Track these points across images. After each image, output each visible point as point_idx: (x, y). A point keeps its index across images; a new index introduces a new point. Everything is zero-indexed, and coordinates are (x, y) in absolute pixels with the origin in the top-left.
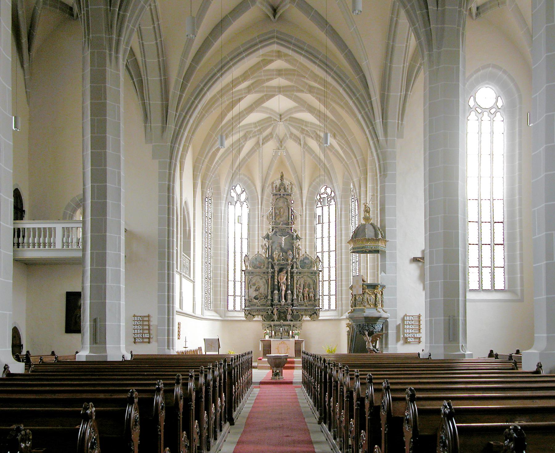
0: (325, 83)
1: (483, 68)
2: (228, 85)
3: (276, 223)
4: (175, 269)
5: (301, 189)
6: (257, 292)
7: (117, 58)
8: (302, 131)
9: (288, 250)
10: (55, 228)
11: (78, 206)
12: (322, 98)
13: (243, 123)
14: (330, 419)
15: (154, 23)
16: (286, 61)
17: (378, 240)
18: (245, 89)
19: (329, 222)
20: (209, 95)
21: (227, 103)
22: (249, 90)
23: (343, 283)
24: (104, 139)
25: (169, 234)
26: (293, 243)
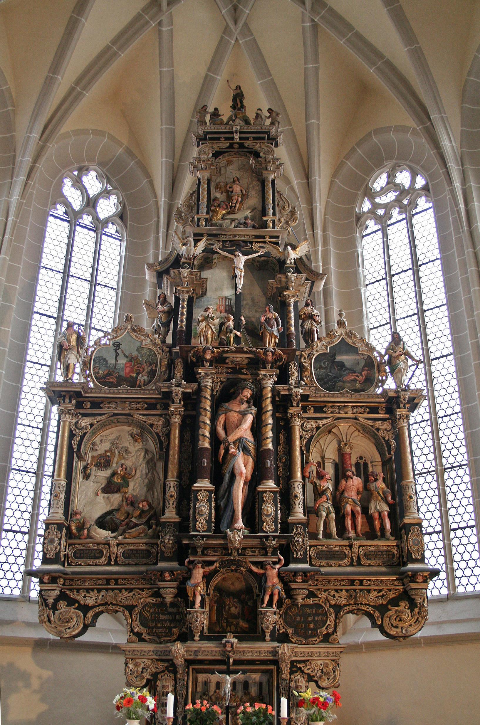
6: (116, 498)
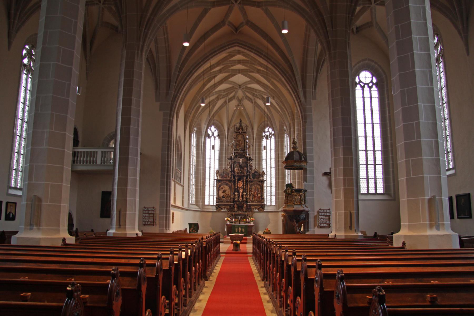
0: (267, 68)
1: (363, 60)
2: (208, 68)
3: (236, 150)
4: (171, 178)
5: (253, 129)
7: (142, 55)
8: (253, 95)
9: (244, 166)
10: (97, 152)
11: (112, 139)
12: (266, 76)
13: (216, 90)
14: (270, 278)
15: (164, 35)
16: (244, 55)
17: (302, 161)
18: (218, 71)
19: (271, 150)
20: (196, 75)
21: (207, 78)
22: (220, 71)
23: (280, 188)
24: (131, 100)
25: (169, 156)
26: (248, 162)
